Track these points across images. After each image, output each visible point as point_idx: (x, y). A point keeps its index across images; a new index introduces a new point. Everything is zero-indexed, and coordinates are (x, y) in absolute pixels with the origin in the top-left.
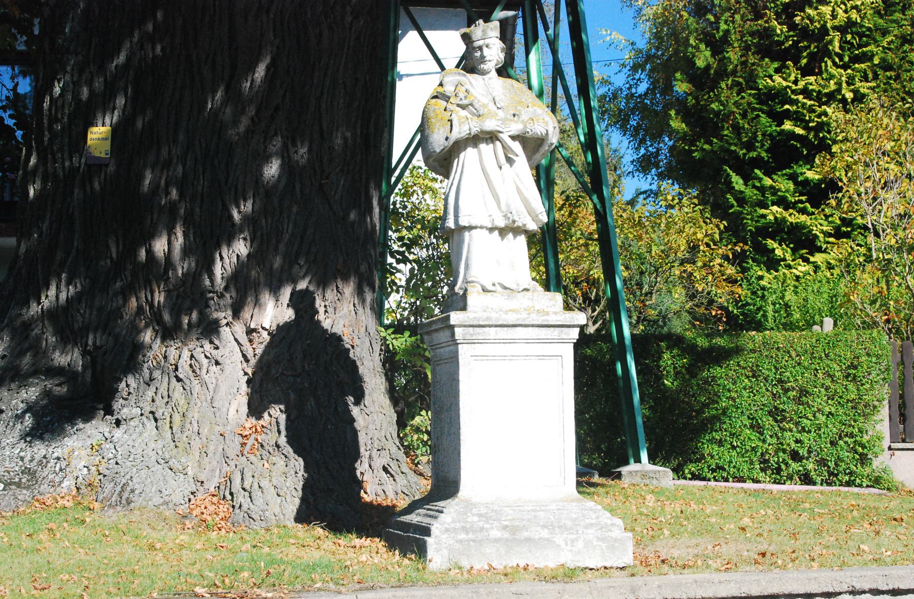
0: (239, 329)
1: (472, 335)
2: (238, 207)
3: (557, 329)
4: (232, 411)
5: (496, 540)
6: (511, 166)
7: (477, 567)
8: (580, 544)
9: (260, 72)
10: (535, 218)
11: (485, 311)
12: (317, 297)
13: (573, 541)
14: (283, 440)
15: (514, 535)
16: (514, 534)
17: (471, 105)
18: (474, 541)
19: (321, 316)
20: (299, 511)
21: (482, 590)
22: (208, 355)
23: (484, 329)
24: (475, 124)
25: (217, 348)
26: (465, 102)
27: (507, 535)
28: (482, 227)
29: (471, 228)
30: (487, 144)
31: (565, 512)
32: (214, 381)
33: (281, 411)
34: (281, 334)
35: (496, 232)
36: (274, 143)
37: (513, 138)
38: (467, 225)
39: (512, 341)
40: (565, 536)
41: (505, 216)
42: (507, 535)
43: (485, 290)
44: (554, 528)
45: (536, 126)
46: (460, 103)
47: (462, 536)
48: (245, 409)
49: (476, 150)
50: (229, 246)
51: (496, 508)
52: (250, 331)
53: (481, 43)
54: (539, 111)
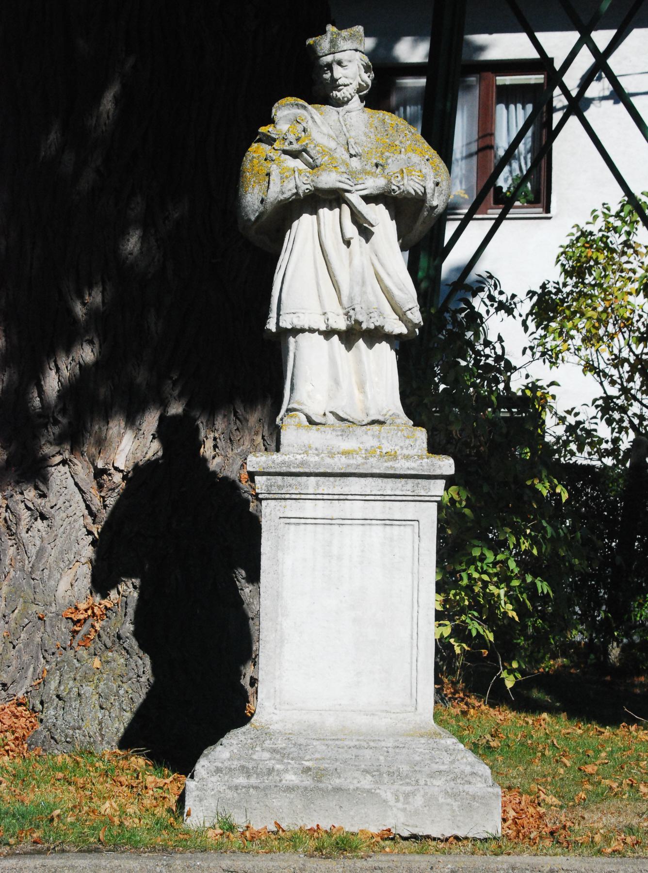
0: (82, 470)
1: (279, 487)
2: (81, 297)
3: (410, 481)
4: (63, 586)
5: (290, 789)
6: (367, 241)
7: (257, 826)
8: (418, 801)
9: (108, 103)
10: (402, 317)
11: (306, 452)
12: (201, 425)
13: (407, 795)
14: (129, 628)
15: (319, 781)
16: (320, 781)
17: (305, 150)
18: (256, 788)
19: (207, 450)
20: (127, 731)
21: (178, 862)
22: (30, 505)
23: (299, 478)
24: (304, 179)
25: (43, 496)
26: (296, 146)
27: (308, 782)
28: (312, 331)
29: (296, 331)
30: (331, 209)
31: (405, 751)
32: (38, 543)
33: (135, 587)
34: (141, 475)
35: (336, 337)
36: (133, 206)
37: (368, 199)
38: (289, 327)
39: (343, 498)
40: (396, 786)
41: (347, 314)
42: (308, 782)
43: (311, 422)
44: (381, 775)
45: (405, 181)
46: (287, 147)
47: (241, 780)
48: (85, 582)
49: (315, 217)
50: (68, 352)
51: (302, 741)
52: (99, 474)
53: (329, 58)
54: (415, 158)
